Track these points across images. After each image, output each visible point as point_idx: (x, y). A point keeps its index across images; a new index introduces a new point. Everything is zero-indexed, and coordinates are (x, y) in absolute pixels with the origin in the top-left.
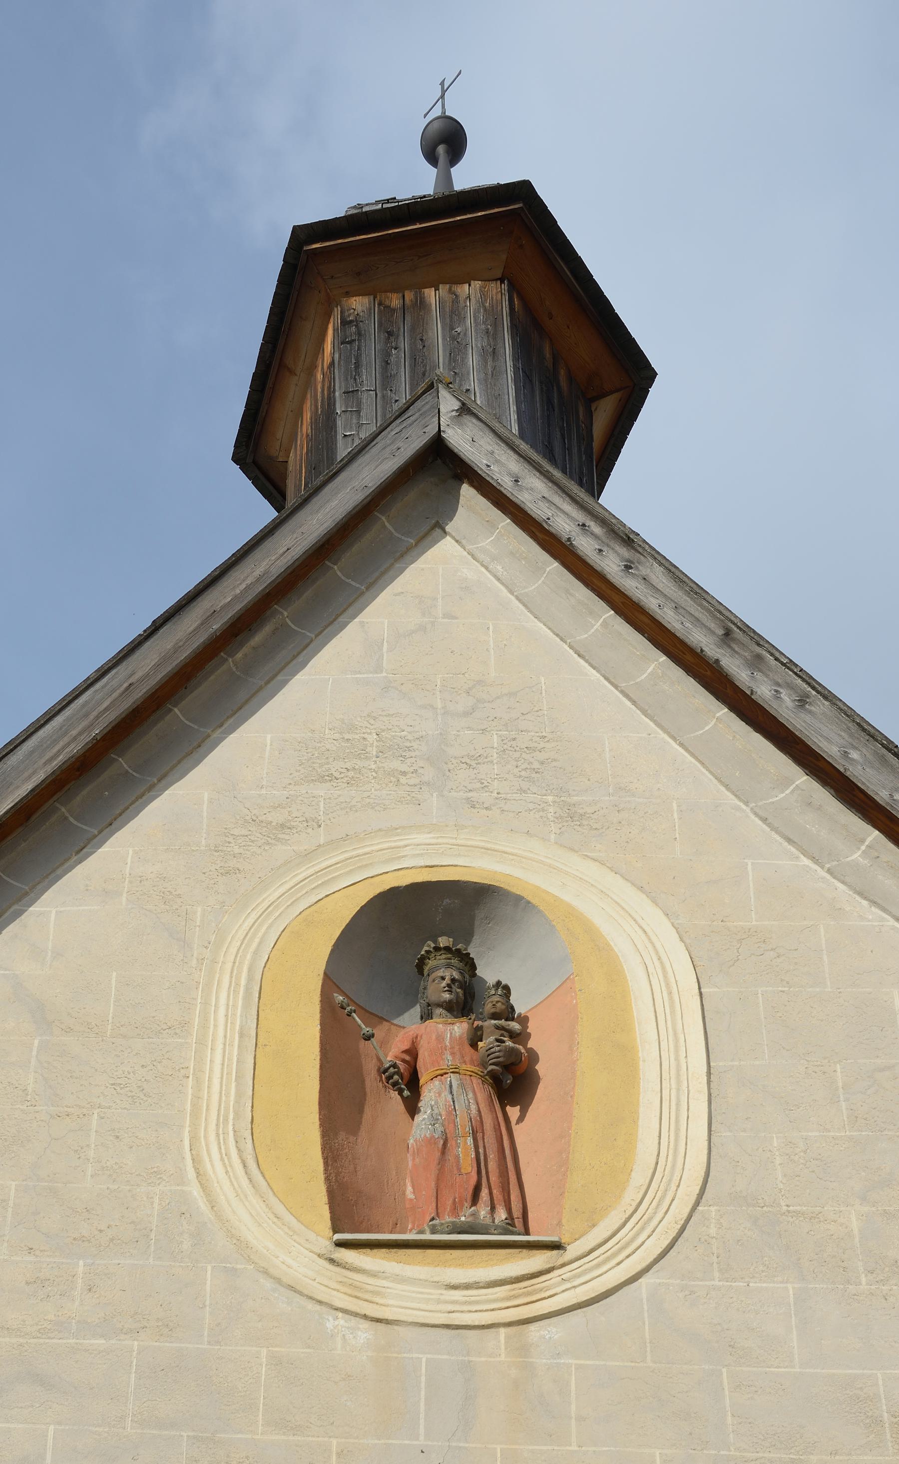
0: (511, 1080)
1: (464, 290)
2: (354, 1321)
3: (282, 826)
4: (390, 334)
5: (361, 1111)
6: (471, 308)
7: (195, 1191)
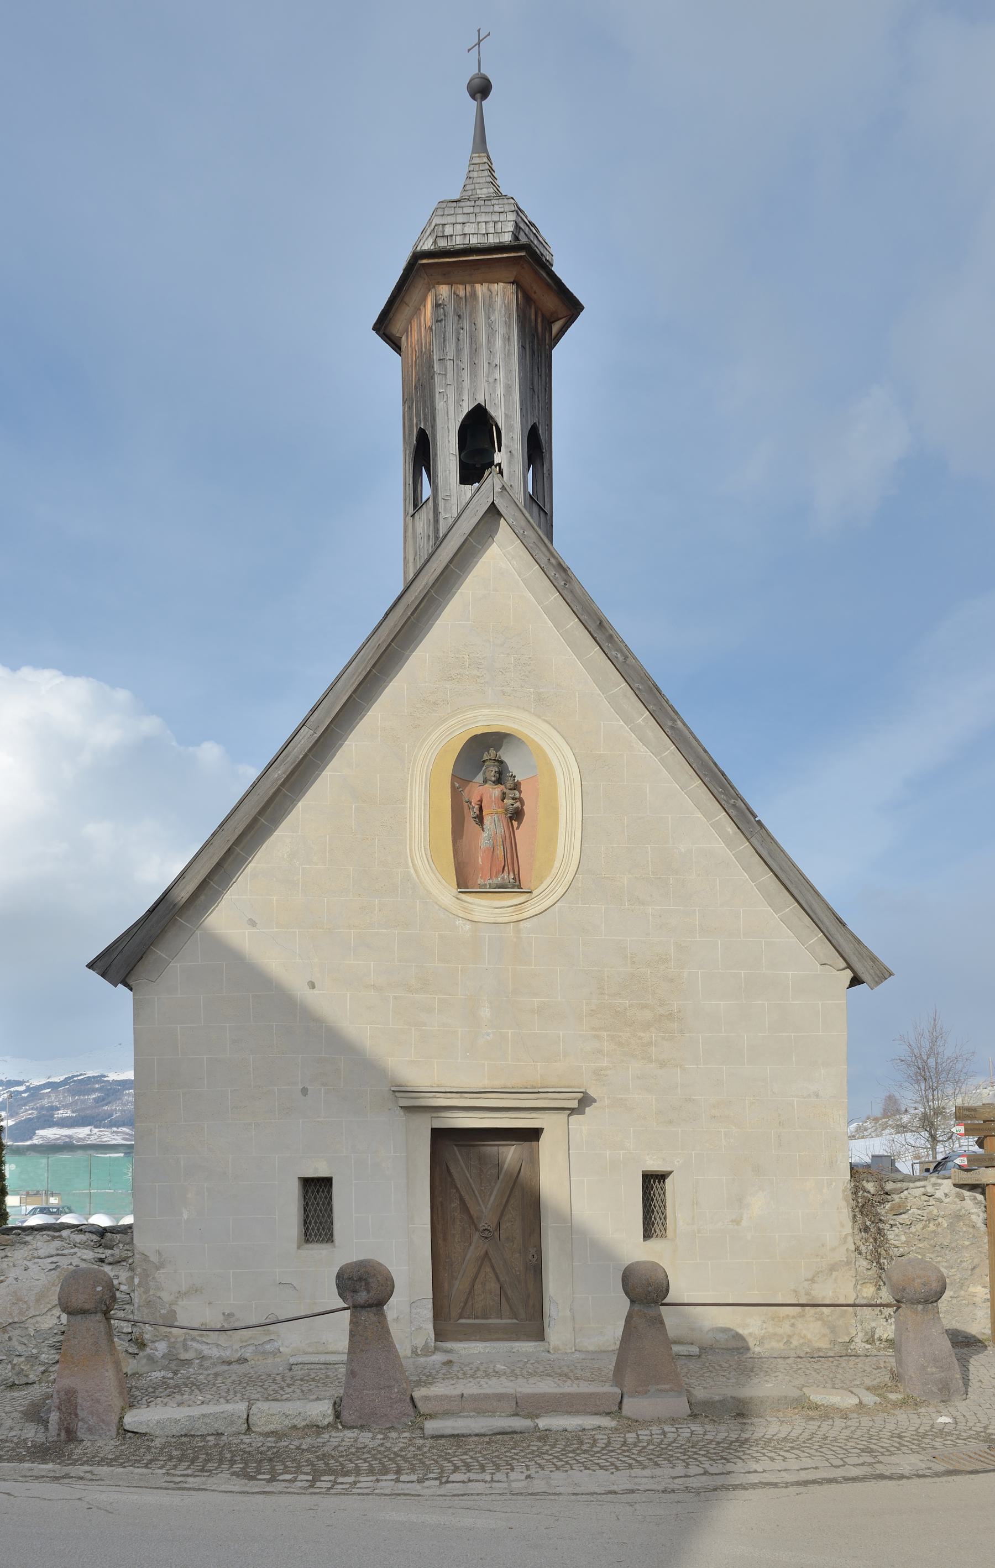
0: (517, 815)
1: (495, 287)
2: (465, 922)
3: (435, 703)
4: (459, 316)
5: (463, 826)
6: (499, 302)
7: (412, 871)
